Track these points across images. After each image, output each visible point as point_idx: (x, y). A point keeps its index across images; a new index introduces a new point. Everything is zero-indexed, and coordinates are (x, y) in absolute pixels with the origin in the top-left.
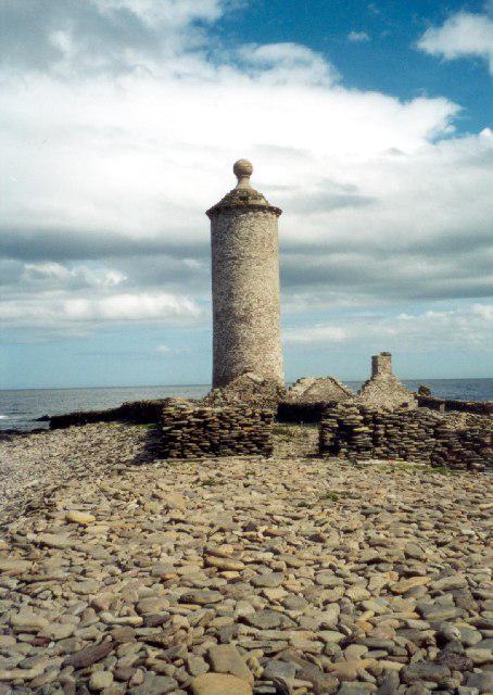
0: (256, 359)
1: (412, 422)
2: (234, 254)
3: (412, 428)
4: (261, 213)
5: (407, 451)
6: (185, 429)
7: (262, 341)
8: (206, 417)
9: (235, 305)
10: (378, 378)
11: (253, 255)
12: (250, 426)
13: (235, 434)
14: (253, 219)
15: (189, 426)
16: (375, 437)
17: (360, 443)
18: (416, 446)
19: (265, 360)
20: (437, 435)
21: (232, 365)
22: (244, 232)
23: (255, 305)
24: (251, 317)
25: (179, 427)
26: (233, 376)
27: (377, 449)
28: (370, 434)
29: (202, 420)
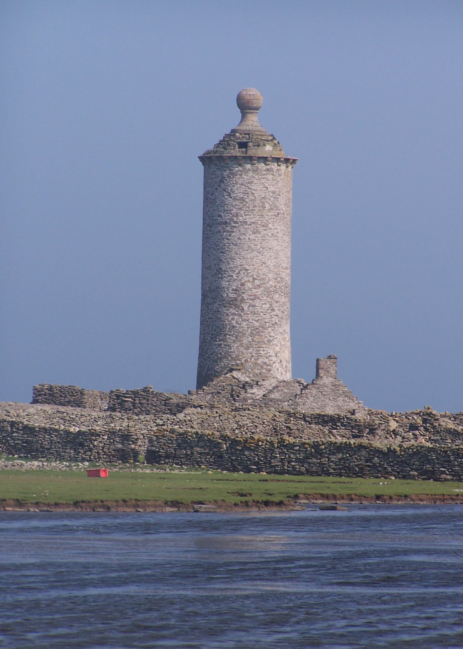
0: (247, 354)
1: (153, 397)
2: (226, 217)
3: (153, 400)
4: (262, 166)
5: (149, 412)
6: (43, 396)
7: (256, 332)
8: (54, 391)
9: (224, 284)
10: (320, 382)
11: (249, 221)
12: (74, 396)
13: (67, 400)
14: (251, 174)
15: (45, 395)
16: (134, 404)
17: (126, 407)
18: (154, 409)
19: (259, 356)
20: (165, 405)
21: (215, 361)
22: (238, 191)
23: (249, 285)
24: (243, 300)
25: (40, 395)
26: (217, 375)
27: (135, 410)
28: (132, 402)
29: (51, 392)
